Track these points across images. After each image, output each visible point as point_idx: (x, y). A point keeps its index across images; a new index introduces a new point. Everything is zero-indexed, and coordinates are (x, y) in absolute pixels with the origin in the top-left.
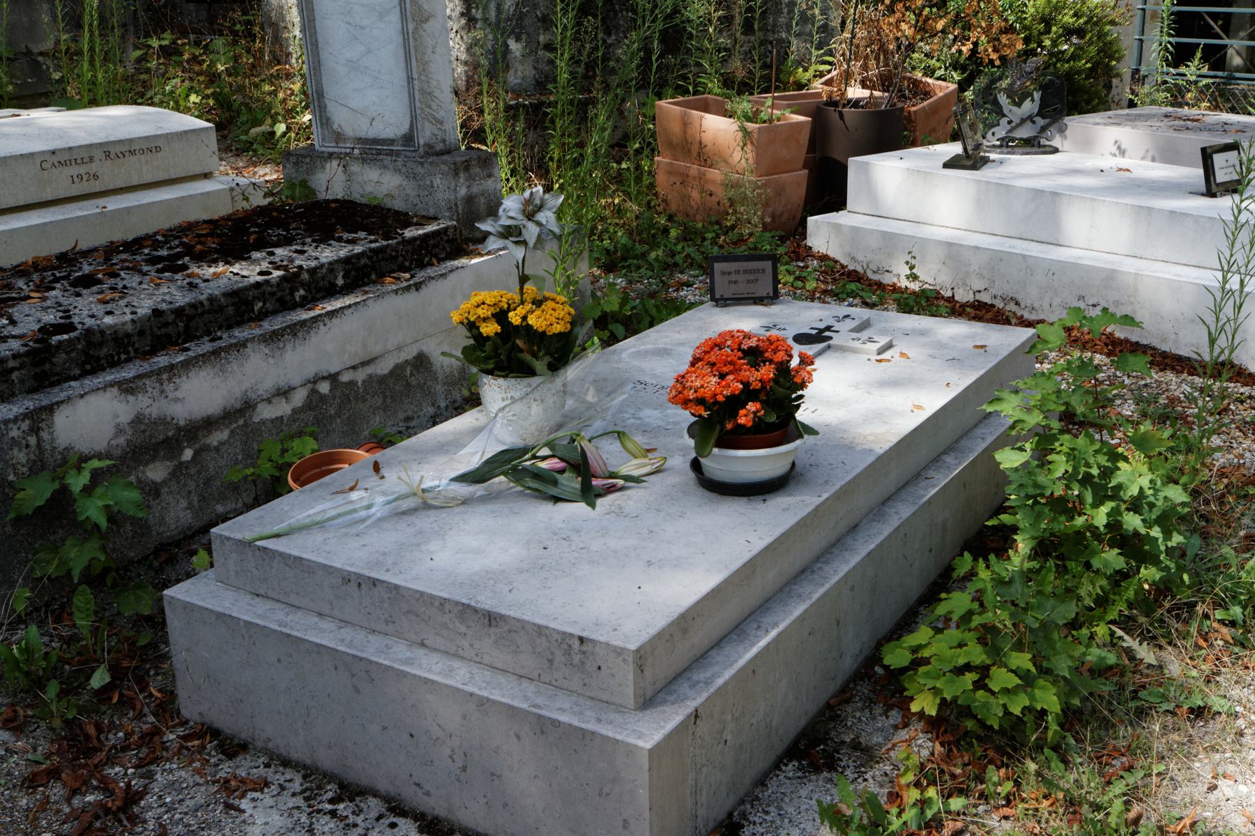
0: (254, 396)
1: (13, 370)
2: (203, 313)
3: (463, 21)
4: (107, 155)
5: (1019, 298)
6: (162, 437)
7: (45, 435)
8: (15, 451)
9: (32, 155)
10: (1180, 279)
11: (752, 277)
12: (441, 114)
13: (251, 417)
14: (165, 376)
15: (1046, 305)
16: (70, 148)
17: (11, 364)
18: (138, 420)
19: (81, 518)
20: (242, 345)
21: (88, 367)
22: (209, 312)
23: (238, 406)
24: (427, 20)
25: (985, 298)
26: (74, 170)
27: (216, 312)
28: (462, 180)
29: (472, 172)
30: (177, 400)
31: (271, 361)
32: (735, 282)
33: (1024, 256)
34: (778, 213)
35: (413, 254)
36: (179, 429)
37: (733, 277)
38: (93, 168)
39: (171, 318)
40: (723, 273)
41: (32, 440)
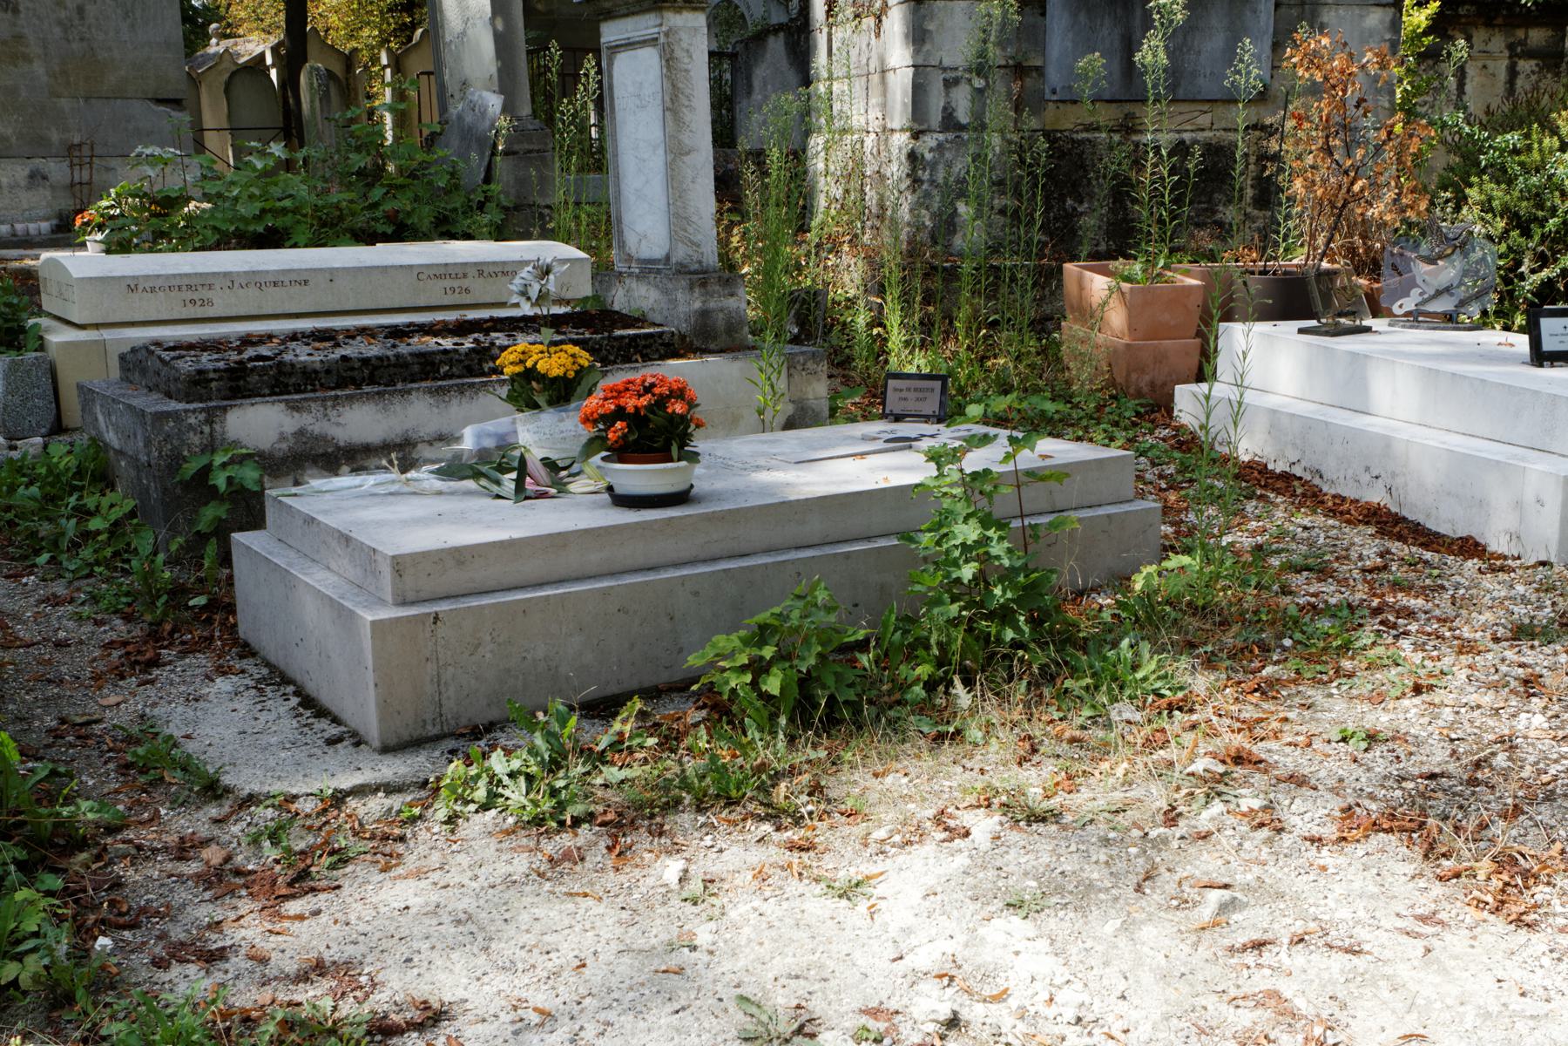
0: (414, 436)
1: (212, 380)
2: (389, 366)
3: (908, 182)
4: (481, 273)
5: (1323, 470)
6: (321, 451)
7: (217, 427)
8: (191, 434)
9: (411, 267)
10: (1478, 454)
11: (921, 395)
12: (698, 238)
13: (410, 453)
14: (329, 403)
15: (1342, 477)
16: (446, 265)
17: (212, 375)
18: (301, 433)
19: (211, 483)
20: (409, 392)
21: (277, 390)
22: (395, 366)
23: (398, 441)
24: (687, 153)
25: (1297, 471)
26: (448, 283)
27: (401, 366)
28: (696, 295)
29: (709, 288)
30: (338, 424)
31: (435, 410)
32: (905, 399)
33: (1326, 423)
34: (1159, 382)
35: (619, 350)
36: (338, 448)
37: (904, 394)
38: (465, 283)
39: (357, 365)
40: (896, 390)
41: (207, 429)
